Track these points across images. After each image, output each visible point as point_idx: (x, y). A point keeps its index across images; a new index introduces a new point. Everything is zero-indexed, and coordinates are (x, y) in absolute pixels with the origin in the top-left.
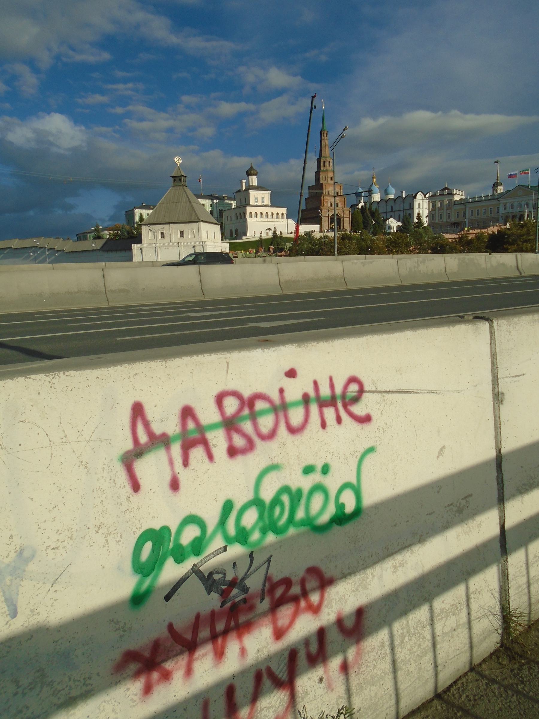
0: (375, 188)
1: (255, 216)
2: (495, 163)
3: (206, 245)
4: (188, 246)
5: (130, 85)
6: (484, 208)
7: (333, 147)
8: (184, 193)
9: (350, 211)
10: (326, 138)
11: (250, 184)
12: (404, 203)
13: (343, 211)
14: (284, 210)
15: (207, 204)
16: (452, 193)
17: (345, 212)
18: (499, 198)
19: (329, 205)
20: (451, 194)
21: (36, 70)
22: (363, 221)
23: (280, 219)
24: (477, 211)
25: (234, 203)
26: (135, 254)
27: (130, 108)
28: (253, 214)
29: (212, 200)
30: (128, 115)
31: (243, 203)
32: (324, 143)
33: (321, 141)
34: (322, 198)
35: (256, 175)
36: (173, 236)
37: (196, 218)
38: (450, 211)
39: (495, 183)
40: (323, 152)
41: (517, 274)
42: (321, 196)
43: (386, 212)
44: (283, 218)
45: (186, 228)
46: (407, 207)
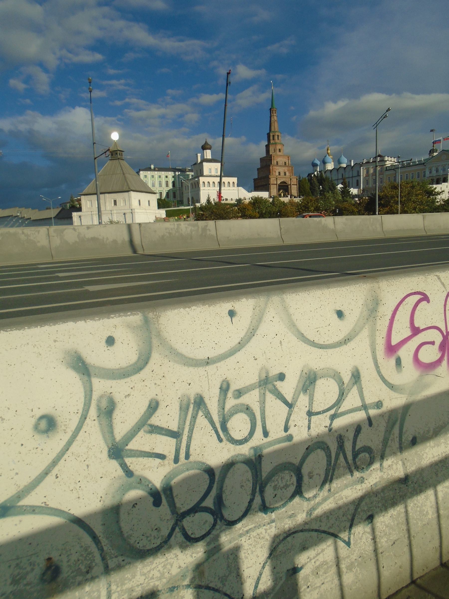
0: (329, 158)
1: (207, 185)
2: (431, 131)
3: (135, 212)
4: (119, 213)
5: (122, 81)
6: (418, 172)
7: (376, 125)
8: (119, 165)
9: (297, 179)
10: (275, 114)
11: (205, 157)
12: (352, 170)
13: (291, 179)
14: (235, 180)
15: (163, 176)
16: (384, 160)
17: (292, 179)
18: (425, 163)
19: (277, 174)
20: (383, 161)
21: (46, 70)
22: (310, 187)
23: (231, 188)
24: (405, 175)
25: (191, 174)
26: (75, 221)
27: (127, 100)
28: (206, 183)
29: (175, 172)
30: (127, 106)
31: (199, 174)
32: (273, 119)
33: (271, 117)
34: (271, 168)
35: (210, 149)
36: (108, 204)
37: (127, 188)
38: (382, 176)
39: (431, 150)
40: (272, 127)
41: (129, 253)
42: (270, 166)
43: (338, 179)
44: (234, 187)
45: (119, 197)
46: (355, 174)
